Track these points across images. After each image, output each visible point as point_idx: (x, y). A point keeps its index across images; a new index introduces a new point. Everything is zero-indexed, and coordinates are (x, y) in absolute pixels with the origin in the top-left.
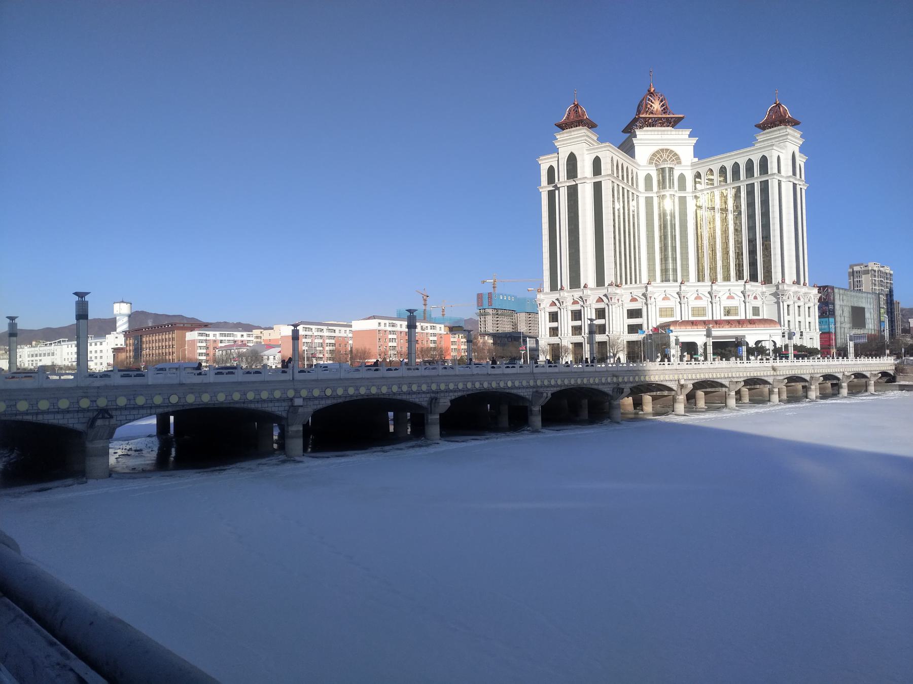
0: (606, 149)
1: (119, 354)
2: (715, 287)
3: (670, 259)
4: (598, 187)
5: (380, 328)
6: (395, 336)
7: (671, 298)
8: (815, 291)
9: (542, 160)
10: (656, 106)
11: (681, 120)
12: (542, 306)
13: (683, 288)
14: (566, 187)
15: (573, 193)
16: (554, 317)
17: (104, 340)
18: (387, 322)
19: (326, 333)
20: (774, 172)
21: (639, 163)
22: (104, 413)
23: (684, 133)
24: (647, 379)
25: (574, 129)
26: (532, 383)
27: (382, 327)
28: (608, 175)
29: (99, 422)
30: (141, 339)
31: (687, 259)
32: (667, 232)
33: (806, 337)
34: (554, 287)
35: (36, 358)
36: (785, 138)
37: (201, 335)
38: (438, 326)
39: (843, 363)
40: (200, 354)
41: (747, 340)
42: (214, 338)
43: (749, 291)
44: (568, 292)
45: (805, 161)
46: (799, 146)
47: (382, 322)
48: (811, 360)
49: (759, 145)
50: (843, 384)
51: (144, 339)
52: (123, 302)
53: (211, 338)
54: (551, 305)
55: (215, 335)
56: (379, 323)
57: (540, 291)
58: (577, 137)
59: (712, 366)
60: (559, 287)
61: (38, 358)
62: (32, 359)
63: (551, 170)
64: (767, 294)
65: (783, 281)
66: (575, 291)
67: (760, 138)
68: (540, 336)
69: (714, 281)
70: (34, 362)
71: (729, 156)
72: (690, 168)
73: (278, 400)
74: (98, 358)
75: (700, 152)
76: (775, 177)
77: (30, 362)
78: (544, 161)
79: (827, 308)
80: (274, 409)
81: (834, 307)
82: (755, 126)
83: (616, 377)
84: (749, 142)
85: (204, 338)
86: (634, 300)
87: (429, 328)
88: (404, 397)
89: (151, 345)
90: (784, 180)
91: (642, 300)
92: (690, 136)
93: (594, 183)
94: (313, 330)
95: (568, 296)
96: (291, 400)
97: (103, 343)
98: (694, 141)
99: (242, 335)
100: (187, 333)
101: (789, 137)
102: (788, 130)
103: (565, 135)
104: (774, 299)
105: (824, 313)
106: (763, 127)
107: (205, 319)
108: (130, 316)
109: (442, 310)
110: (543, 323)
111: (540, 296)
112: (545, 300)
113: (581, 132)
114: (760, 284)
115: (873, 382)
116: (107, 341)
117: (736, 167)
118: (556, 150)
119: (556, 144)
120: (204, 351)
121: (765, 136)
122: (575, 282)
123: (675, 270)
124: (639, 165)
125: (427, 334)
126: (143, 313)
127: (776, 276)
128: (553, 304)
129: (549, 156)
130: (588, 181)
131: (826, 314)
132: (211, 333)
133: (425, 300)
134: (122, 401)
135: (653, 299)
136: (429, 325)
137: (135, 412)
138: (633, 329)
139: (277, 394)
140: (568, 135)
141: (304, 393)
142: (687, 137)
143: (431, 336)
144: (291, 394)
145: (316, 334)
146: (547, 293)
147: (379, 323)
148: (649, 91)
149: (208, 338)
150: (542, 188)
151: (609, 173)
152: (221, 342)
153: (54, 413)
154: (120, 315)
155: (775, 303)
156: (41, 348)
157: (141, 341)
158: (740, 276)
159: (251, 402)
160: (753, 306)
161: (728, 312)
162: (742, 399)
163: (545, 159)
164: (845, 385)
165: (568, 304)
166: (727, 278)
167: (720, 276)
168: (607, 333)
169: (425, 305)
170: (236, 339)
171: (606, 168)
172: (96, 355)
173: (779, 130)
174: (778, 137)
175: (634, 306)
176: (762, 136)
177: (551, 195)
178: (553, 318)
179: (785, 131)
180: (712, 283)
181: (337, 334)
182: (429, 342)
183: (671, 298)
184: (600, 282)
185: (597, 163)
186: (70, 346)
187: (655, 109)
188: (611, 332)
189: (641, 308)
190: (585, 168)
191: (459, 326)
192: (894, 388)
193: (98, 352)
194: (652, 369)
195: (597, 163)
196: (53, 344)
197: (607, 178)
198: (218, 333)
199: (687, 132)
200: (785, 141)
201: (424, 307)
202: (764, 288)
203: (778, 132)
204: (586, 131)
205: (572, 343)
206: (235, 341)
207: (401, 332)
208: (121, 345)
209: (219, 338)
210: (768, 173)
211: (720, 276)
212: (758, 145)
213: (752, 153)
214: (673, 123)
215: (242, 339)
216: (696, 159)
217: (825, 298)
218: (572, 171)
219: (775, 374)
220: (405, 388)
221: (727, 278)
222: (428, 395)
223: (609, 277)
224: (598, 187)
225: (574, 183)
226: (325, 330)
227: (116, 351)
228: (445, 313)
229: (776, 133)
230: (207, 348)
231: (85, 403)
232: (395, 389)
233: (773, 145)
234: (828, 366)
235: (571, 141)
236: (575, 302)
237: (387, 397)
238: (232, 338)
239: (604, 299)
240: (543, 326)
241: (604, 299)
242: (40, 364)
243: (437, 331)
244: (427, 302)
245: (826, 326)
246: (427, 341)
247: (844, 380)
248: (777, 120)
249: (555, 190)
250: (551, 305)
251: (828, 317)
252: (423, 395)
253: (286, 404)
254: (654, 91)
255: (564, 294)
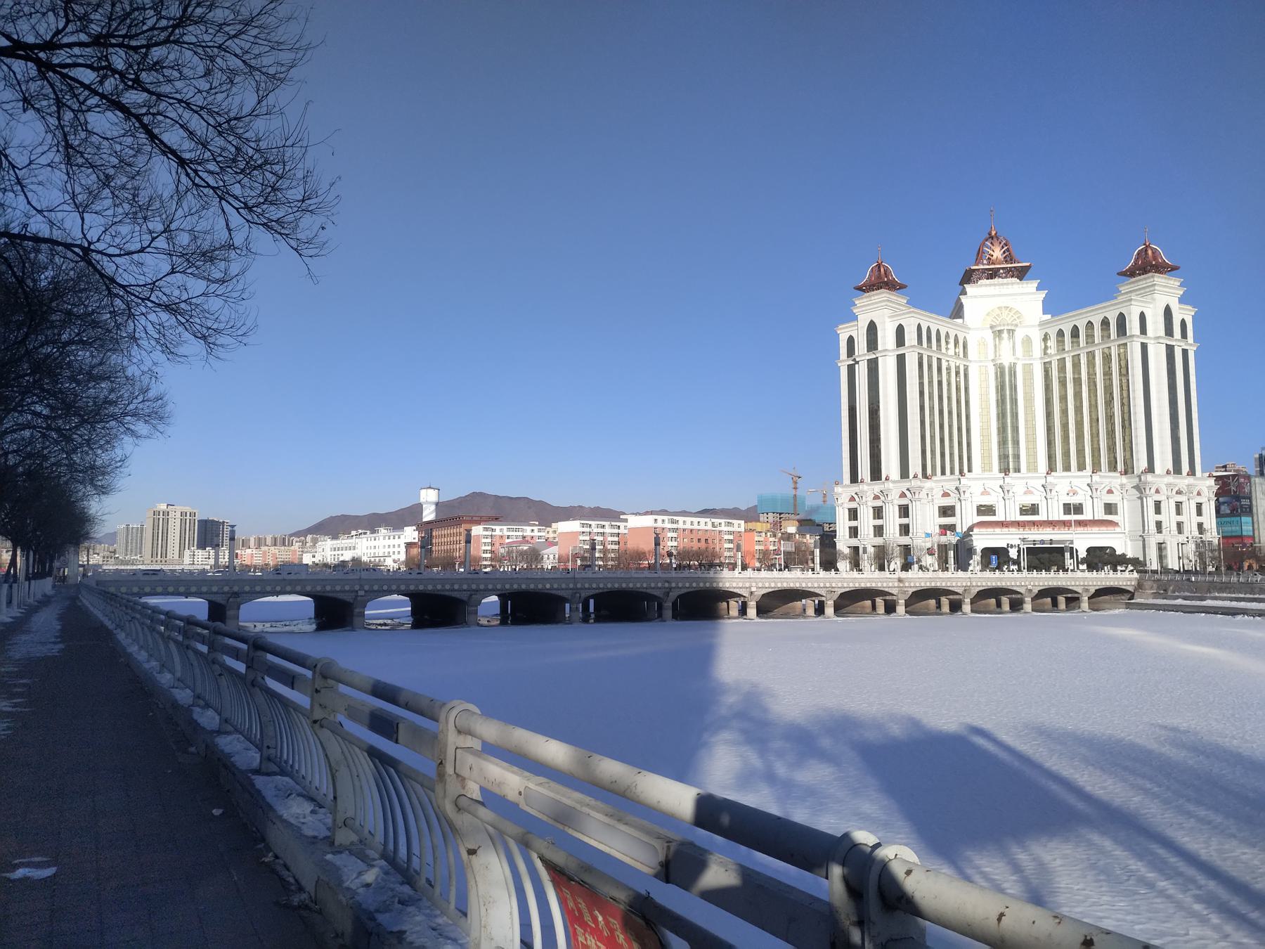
0: (910, 315)
1: (411, 550)
2: (1050, 479)
3: (1010, 442)
4: (901, 360)
5: (655, 525)
6: (674, 535)
7: (1035, 491)
8: (1212, 482)
9: (841, 329)
10: (997, 253)
11: (1028, 271)
12: (840, 502)
13: (963, 481)
14: (866, 361)
15: (873, 366)
16: (853, 514)
17: (402, 533)
18: (666, 518)
19: (608, 530)
20: (1133, 334)
21: (969, 326)
22: (236, 595)
23: (1029, 285)
24: (721, 585)
25: (875, 292)
26: (571, 586)
27: (659, 524)
28: (912, 346)
29: (231, 600)
30: (431, 533)
31: (1034, 441)
32: (1006, 409)
33: (1171, 542)
34: (854, 478)
35: (338, 552)
36: (1151, 289)
37: (486, 529)
38: (736, 522)
39: (1028, 576)
40: (485, 552)
41: (1075, 546)
42: (501, 534)
43: (1097, 483)
44: (868, 485)
45: (1193, 314)
46: (1179, 296)
47: (660, 518)
48: (1052, 573)
49: (1122, 297)
50: (1026, 599)
51: (434, 534)
52: (430, 488)
53: (498, 533)
54: (850, 500)
55: (501, 530)
56: (656, 520)
57: (837, 483)
58: (876, 303)
59: (953, 576)
60: (860, 478)
61: (340, 552)
62: (335, 553)
63: (851, 341)
64: (1129, 487)
65: (1151, 468)
66: (876, 484)
67: (1124, 289)
68: (837, 537)
69: (1096, 467)
70: (336, 557)
71: (1104, 307)
72: (1038, 328)
73: (348, 591)
74: (396, 553)
75: (1049, 307)
76: (1135, 339)
77: (333, 557)
78: (843, 331)
79: (1238, 504)
80: (345, 598)
81: (1251, 502)
82: (1118, 274)
83: (668, 582)
84: (1110, 294)
85: (489, 533)
86: (946, 495)
87: (723, 524)
88: (447, 593)
89: (452, 538)
90: (1152, 342)
91: (955, 495)
92: (1038, 289)
93: (898, 355)
94: (593, 526)
95: (868, 488)
96: (357, 591)
97: (401, 537)
98: (1042, 294)
99: (533, 530)
100: (473, 528)
101: (1156, 288)
102: (1156, 279)
103: (865, 300)
104: (1137, 493)
105: (1234, 510)
106: (1131, 273)
107: (556, 501)
108: (437, 504)
109: (823, 495)
110: (866, 520)
111: (838, 489)
112: (843, 493)
113: (882, 295)
114: (1119, 474)
115: (1086, 598)
116: (405, 534)
117: (1105, 323)
118: (855, 318)
119: (854, 311)
120: (489, 548)
121: (1129, 286)
122: (876, 474)
123: (1017, 457)
124: (970, 329)
125: (720, 532)
126: (481, 495)
127: (1141, 462)
128: (852, 499)
129: (847, 325)
130: (890, 354)
131: (1237, 511)
132: (498, 528)
133: (796, 483)
134: (247, 589)
135: (967, 494)
136: (723, 521)
137: (255, 595)
138: (945, 529)
139: (347, 588)
140: (868, 299)
141: (366, 588)
142: (1034, 290)
143: (726, 534)
144: (357, 588)
145: (596, 530)
146: (846, 486)
147: (656, 520)
148: (990, 234)
149: (494, 533)
150: (841, 362)
151: (913, 344)
152: (508, 538)
153: (210, 594)
154: (427, 502)
155: (1138, 498)
156: (343, 541)
157: (431, 536)
158: (1081, 467)
159: (329, 592)
160: (1065, 502)
161: (1067, 508)
162: (877, 610)
163: (844, 328)
164: (1028, 599)
165: (868, 499)
166: (1067, 468)
167: (1059, 465)
168: (910, 534)
169: (795, 488)
170: (525, 534)
171: (911, 337)
172: (394, 550)
173: (1145, 279)
174: (1144, 288)
175: (947, 502)
176: (1126, 287)
177: (851, 370)
178: (949, 512)
179: (1152, 280)
180: (1093, 473)
181: (681, 525)
182: (723, 541)
183: (1035, 491)
184: (904, 473)
185: (900, 331)
186: (369, 539)
187: (995, 257)
188: (915, 534)
189: (954, 504)
190: (887, 338)
191: (810, 520)
192: (1121, 606)
193: (396, 546)
194: (726, 576)
195: (900, 331)
196: (354, 537)
197: (911, 350)
198: (505, 528)
199: (1035, 284)
200: (1153, 292)
201: (793, 492)
202: (1124, 479)
203: (1144, 282)
204: (888, 296)
205: (849, 547)
206: (524, 537)
207: (684, 530)
208: (414, 539)
209: (506, 533)
210: (1126, 335)
211: (1059, 465)
212: (1120, 299)
213: (1107, 309)
214: (1021, 274)
215: (532, 534)
216: (1049, 317)
217: (1235, 490)
218: (872, 344)
219: (902, 585)
220: (448, 587)
221: (1067, 468)
222: (469, 593)
223: (915, 466)
224: (901, 360)
225: (874, 356)
226: (607, 527)
227: (409, 545)
228: (827, 499)
229: (1141, 283)
230: (493, 545)
231: (226, 589)
232: (439, 587)
233: (1131, 300)
234: (1001, 579)
235: (871, 307)
236: (876, 497)
237: (432, 592)
238: (520, 534)
239: (907, 493)
240: (892, 523)
241: (907, 493)
242: (341, 559)
243: (736, 529)
244: (798, 485)
245: (1237, 528)
246: (720, 540)
247: (1027, 594)
248: (1146, 266)
249: (854, 364)
250: (850, 500)
251: (1240, 516)
252: (464, 593)
253: (353, 594)
254: (996, 234)
255: (864, 487)
